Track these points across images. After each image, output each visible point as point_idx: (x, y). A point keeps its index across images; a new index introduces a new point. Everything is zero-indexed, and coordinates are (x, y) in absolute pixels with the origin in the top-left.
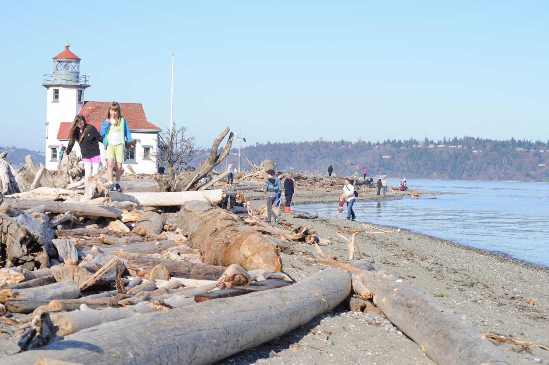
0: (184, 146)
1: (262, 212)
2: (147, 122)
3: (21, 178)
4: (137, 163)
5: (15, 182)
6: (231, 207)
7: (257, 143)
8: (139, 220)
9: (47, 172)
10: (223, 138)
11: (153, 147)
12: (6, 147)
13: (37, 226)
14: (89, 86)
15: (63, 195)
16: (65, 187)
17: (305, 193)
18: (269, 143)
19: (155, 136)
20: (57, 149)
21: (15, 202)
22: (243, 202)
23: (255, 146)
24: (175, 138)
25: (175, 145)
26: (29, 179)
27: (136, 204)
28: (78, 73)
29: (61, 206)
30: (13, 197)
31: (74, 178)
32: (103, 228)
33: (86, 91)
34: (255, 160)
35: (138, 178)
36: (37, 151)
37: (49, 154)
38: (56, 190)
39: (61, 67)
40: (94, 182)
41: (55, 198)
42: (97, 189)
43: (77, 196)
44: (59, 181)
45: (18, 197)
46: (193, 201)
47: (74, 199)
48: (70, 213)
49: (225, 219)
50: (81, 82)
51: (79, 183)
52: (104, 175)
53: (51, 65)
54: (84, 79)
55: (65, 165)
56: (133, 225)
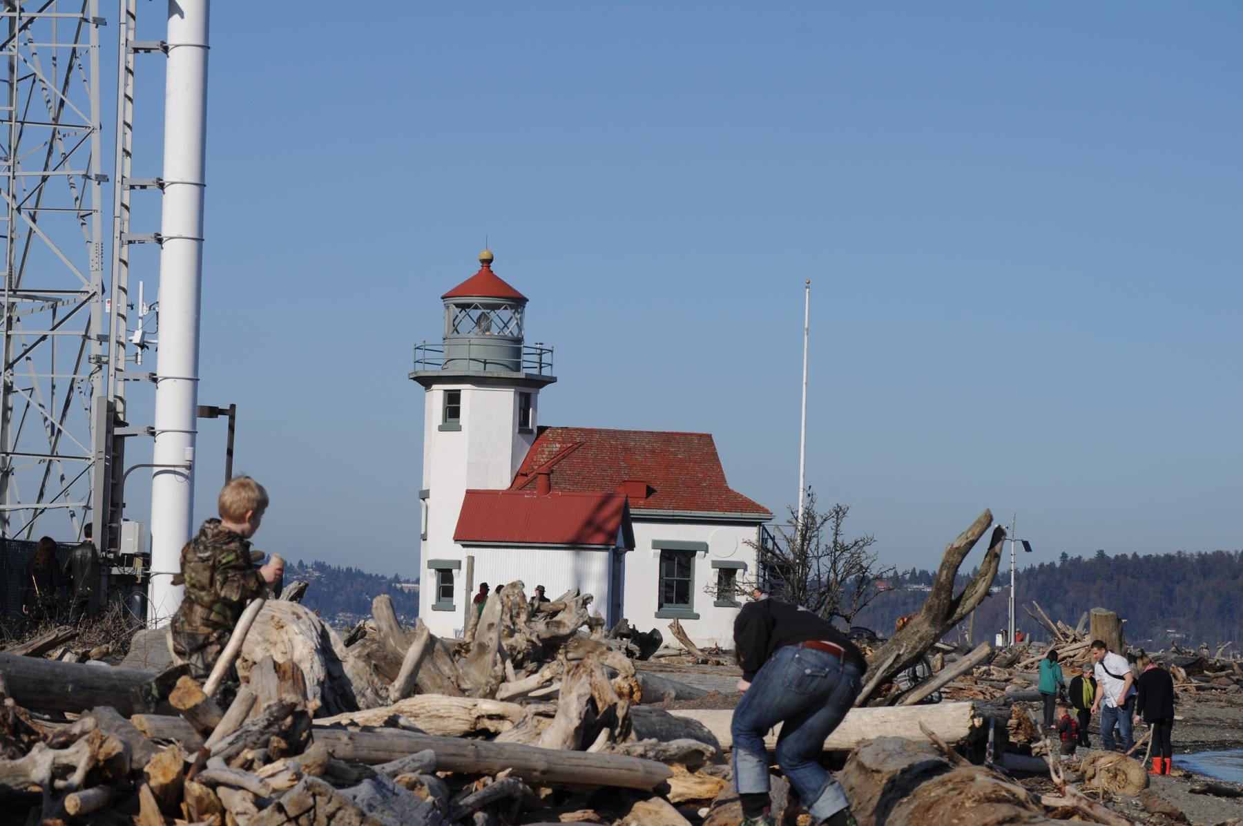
0: (840, 564)
1: (1090, 772)
2: (728, 490)
3: (361, 664)
4: (697, 617)
5: (342, 676)
6: (996, 757)
7: (1064, 556)
8: (721, 797)
9: (438, 646)
10: (972, 543)
11: (745, 567)
12: (296, 565)
13: (415, 815)
14: (552, 380)
15: (491, 717)
16: (491, 694)
17: (1220, 714)
18: (1101, 553)
19: (752, 533)
20: (455, 572)
21: (345, 739)
22: (1030, 742)
23: (1058, 564)
24: (814, 540)
25: (814, 562)
26: (384, 666)
27: (712, 749)
28: (518, 341)
29: (484, 753)
30: (338, 725)
31: (518, 666)
32: (612, 822)
33: (544, 396)
34: (1058, 607)
35: (705, 662)
36: (390, 576)
37: (428, 586)
38: (468, 702)
39: (466, 324)
40: (585, 679)
41: (466, 727)
42: (592, 701)
43: (532, 722)
44: (475, 673)
45: (353, 724)
46: (882, 739)
47: (523, 730)
48: (510, 775)
49: (989, 800)
50: (529, 367)
51: (534, 680)
52: (610, 655)
53: (438, 318)
54: (536, 358)
55: (491, 625)
56: (703, 812)
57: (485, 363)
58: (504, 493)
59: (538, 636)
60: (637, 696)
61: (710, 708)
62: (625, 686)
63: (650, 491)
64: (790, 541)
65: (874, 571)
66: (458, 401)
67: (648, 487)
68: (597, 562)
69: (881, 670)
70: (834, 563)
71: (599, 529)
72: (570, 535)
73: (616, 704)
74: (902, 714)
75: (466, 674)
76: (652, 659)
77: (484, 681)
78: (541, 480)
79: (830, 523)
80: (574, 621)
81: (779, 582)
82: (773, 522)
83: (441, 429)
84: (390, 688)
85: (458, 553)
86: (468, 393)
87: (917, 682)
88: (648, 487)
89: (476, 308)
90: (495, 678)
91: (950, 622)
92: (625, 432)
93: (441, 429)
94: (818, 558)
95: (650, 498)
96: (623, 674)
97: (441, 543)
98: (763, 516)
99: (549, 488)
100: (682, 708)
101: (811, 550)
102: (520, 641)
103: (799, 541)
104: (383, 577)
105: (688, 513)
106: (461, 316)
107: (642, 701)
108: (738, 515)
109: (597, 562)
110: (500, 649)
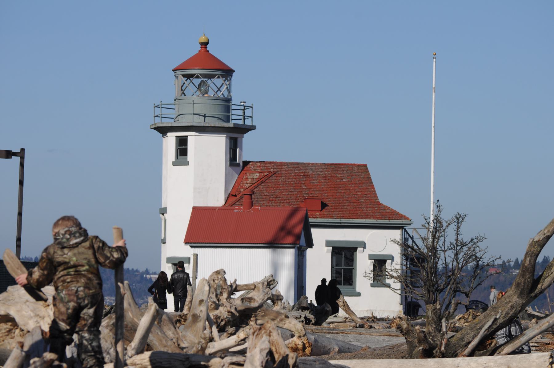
0: (461, 256)
2: (379, 204)
4: (359, 295)
11: (392, 259)
14: (253, 128)
19: (397, 234)
25: (442, 254)
28: (228, 100)
31: (221, 330)
33: (247, 139)
35: (362, 326)
39: (191, 89)
40: (265, 338)
42: (270, 353)
50: (236, 120)
51: (233, 340)
52: (287, 321)
53: (171, 85)
55: (201, 301)
57: (205, 116)
58: (219, 208)
59: (236, 309)
60: (308, 351)
61: (361, 358)
62: (300, 343)
63: (324, 206)
64: (424, 239)
65: (486, 260)
66: (186, 144)
67: (322, 202)
68: (288, 256)
69: (483, 330)
70: (457, 255)
71: (289, 233)
72: (269, 237)
73: (287, 355)
74: (499, 361)
75: (184, 336)
76: (324, 325)
77: (197, 341)
78: (246, 199)
79: (453, 226)
80: (261, 297)
81: (417, 269)
82: (412, 226)
83: (174, 164)
84: (128, 348)
85: (187, 252)
86: (193, 138)
87: (511, 338)
88: (322, 202)
89: (197, 77)
90: (205, 339)
91: (533, 295)
92: (305, 164)
93: (174, 164)
94: (445, 251)
95: (324, 211)
96: (297, 335)
97: (175, 246)
98: (405, 222)
99: (252, 205)
100: (342, 358)
101: (440, 245)
102: (223, 312)
103: (431, 240)
104: (137, 271)
105: (351, 221)
106: (187, 83)
107: (311, 354)
108: (386, 221)
109: (288, 256)
110: (208, 319)
